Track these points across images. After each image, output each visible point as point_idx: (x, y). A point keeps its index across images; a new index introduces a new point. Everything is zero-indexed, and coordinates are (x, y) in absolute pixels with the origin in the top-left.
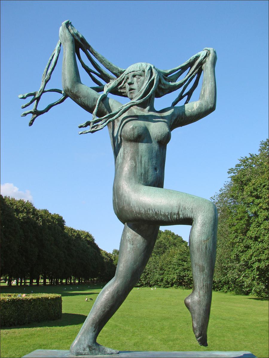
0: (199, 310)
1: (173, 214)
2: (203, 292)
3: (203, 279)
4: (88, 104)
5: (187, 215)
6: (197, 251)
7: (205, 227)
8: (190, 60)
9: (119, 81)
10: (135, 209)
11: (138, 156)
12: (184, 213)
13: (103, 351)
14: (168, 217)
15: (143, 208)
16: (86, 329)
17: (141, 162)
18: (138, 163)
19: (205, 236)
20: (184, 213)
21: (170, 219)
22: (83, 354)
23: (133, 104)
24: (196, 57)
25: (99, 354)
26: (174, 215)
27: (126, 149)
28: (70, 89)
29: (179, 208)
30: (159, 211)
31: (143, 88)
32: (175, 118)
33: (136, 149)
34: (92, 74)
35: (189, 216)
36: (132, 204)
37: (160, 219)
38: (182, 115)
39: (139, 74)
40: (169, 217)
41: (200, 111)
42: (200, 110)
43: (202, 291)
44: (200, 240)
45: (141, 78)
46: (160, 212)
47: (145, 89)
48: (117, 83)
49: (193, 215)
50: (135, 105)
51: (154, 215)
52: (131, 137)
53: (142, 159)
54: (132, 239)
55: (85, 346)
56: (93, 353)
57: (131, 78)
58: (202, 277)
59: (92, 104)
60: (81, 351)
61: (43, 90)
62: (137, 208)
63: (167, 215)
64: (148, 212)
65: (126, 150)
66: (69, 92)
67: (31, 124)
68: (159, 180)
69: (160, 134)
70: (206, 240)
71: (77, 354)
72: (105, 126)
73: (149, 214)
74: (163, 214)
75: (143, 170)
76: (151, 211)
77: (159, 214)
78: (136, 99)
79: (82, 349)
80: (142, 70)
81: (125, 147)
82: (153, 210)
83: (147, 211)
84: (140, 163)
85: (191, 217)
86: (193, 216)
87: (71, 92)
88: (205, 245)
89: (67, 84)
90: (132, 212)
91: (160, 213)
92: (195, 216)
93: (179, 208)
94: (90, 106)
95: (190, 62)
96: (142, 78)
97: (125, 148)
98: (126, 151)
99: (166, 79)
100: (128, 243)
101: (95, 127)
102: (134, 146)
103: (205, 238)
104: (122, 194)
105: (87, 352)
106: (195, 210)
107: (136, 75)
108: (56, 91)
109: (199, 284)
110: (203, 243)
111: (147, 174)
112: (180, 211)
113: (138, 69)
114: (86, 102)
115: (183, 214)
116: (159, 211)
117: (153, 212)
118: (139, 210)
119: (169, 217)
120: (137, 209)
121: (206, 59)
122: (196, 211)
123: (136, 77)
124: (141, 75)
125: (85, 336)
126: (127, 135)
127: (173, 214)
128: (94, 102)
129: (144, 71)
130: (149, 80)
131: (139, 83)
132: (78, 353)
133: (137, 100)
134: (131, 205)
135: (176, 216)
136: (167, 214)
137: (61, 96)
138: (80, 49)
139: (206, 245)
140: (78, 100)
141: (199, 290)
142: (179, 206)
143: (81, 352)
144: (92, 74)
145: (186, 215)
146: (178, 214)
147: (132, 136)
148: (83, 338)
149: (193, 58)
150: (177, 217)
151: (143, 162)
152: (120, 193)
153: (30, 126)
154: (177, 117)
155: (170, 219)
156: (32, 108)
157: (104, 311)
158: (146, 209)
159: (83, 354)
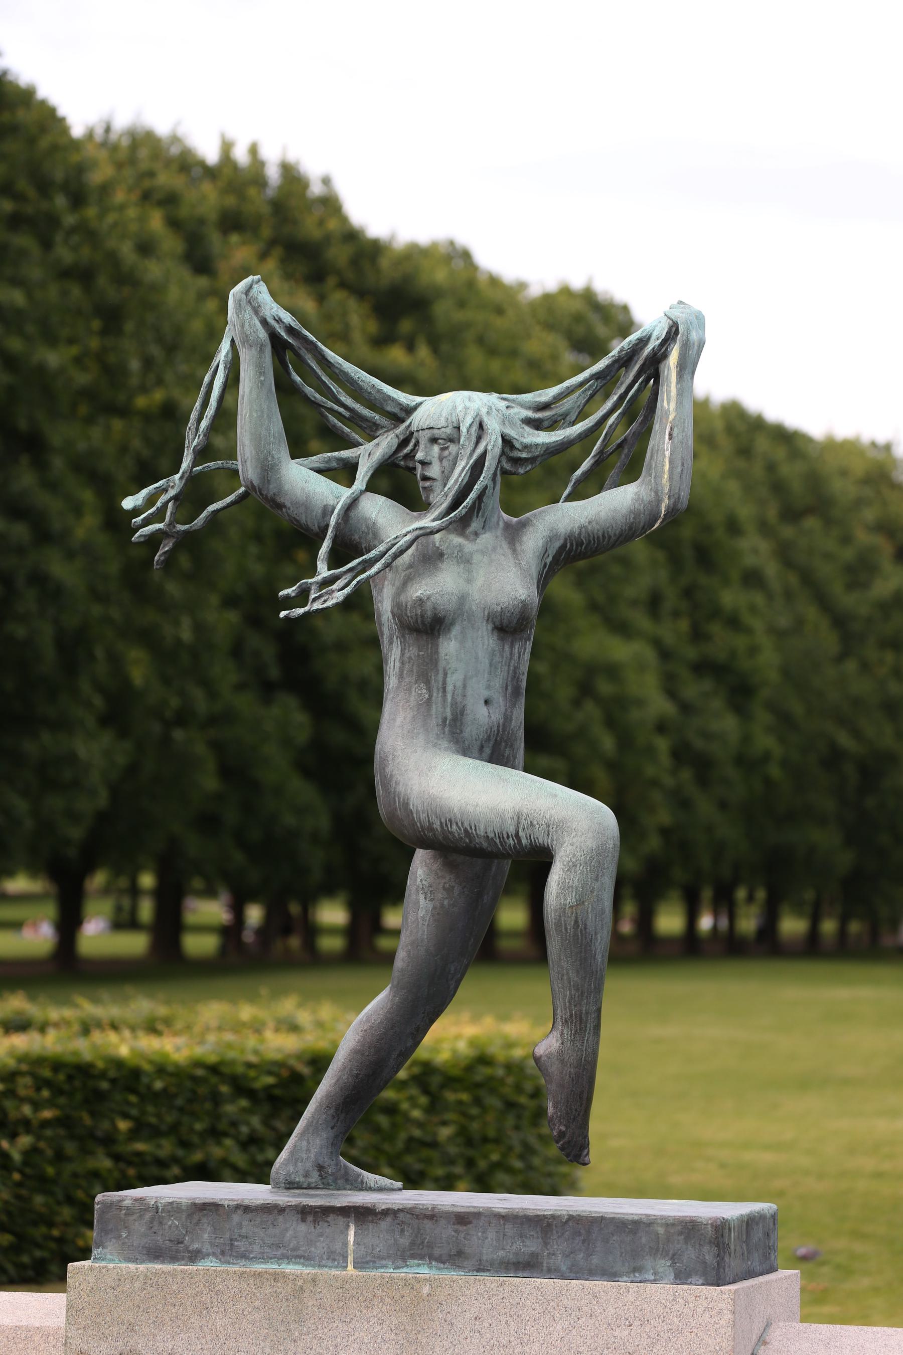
0: (561, 1073)
1: (505, 836)
2: (571, 1030)
3: (571, 998)
4: (309, 523)
5: (537, 841)
6: (556, 930)
7: (576, 872)
8: (621, 350)
9: (402, 438)
10: (420, 818)
11: (438, 671)
12: (530, 836)
13: (356, 1181)
14: (496, 843)
15: (437, 817)
16: (312, 1122)
18: (435, 690)
19: (574, 894)
20: (530, 836)
21: (500, 846)
22: (305, 1185)
23: (421, 532)
24: (638, 339)
25: (345, 1189)
26: (508, 837)
27: (407, 651)
28: (259, 488)
29: (518, 823)
30: (473, 828)
32: (558, 544)
33: (431, 652)
35: (541, 841)
36: (413, 805)
37: (477, 846)
38: (580, 534)
39: (445, 438)
40: (498, 841)
41: (632, 520)
43: (568, 1027)
44: (561, 903)
46: (475, 830)
47: (457, 487)
48: (395, 443)
49: (549, 841)
51: (463, 836)
52: (417, 621)
53: (448, 679)
54: (431, 886)
55: (309, 1165)
56: (328, 1184)
57: (426, 447)
58: (568, 993)
59: (319, 523)
60: (299, 1179)
61: (188, 473)
62: (424, 815)
63: (492, 838)
64: (448, 828)
65: (407, 655)
66: (256, 493)
69: (499, 609)
70: (577, 905)
71: (288, 1186)
73: (451, 833)
74: (482, 834)
75: (448, 710)
76: (454, 827)
77: (472, 833)
79: (301, 1172)
80: (431, 466)
81: (405, 645)
82: (460, 824)
83: (446, 825)
84: (441, 690)
85: (546, 844)
86: (549, 844)
87: (261, 494)
88: (573, 918)
89: (249, 473)
90: (414, 824)
91: (474, 832)
92: (555, 842)
93: (518, 823)
94: (315, 528)
95: (619, 356)
96: (453, 448)
97: (405, 649)
98: (408, 656)
100: (422, 897)
101: (323, 599)
102: (428, 645)
103: (574, 900)
104: (391, 775)
106: (554, 829)
107: (438, 439)
109: (562, 1011)
110: (568, 912)
111: (461, 720)
112: (520, 830)
113: (442, 423)
114: (304, 518)
115: (529, 838)
116: (473, 828)
117: (460, 829)
118: (429, 821)
119: (498, 841)
121: (667, 349)
122: (556, 831)
123: (439, 444)
124: (451, 440)
125: (308, 1140)
126: (408, 617)
127: (505, 836)
128: (323, 518)
129: (458, 428)
131: (445, 463)
132: (290, 1183)
134: (411, 807)
135: (513, 840)
136: (491, 835)
139: (576, 917)
140: (283, 513)
143: (297, 1180)
145: (535, 840)
146: (517, 835)
147: (419, 621)
148: (305, 1143)
149: (629, 344)
150: (515, 843)
151: (450, 688)
152: (387, 770)
154: (566, 540)
155: (500, 846)
157: (357, 1075)
158: (443, 821)
159: (304, 1186)
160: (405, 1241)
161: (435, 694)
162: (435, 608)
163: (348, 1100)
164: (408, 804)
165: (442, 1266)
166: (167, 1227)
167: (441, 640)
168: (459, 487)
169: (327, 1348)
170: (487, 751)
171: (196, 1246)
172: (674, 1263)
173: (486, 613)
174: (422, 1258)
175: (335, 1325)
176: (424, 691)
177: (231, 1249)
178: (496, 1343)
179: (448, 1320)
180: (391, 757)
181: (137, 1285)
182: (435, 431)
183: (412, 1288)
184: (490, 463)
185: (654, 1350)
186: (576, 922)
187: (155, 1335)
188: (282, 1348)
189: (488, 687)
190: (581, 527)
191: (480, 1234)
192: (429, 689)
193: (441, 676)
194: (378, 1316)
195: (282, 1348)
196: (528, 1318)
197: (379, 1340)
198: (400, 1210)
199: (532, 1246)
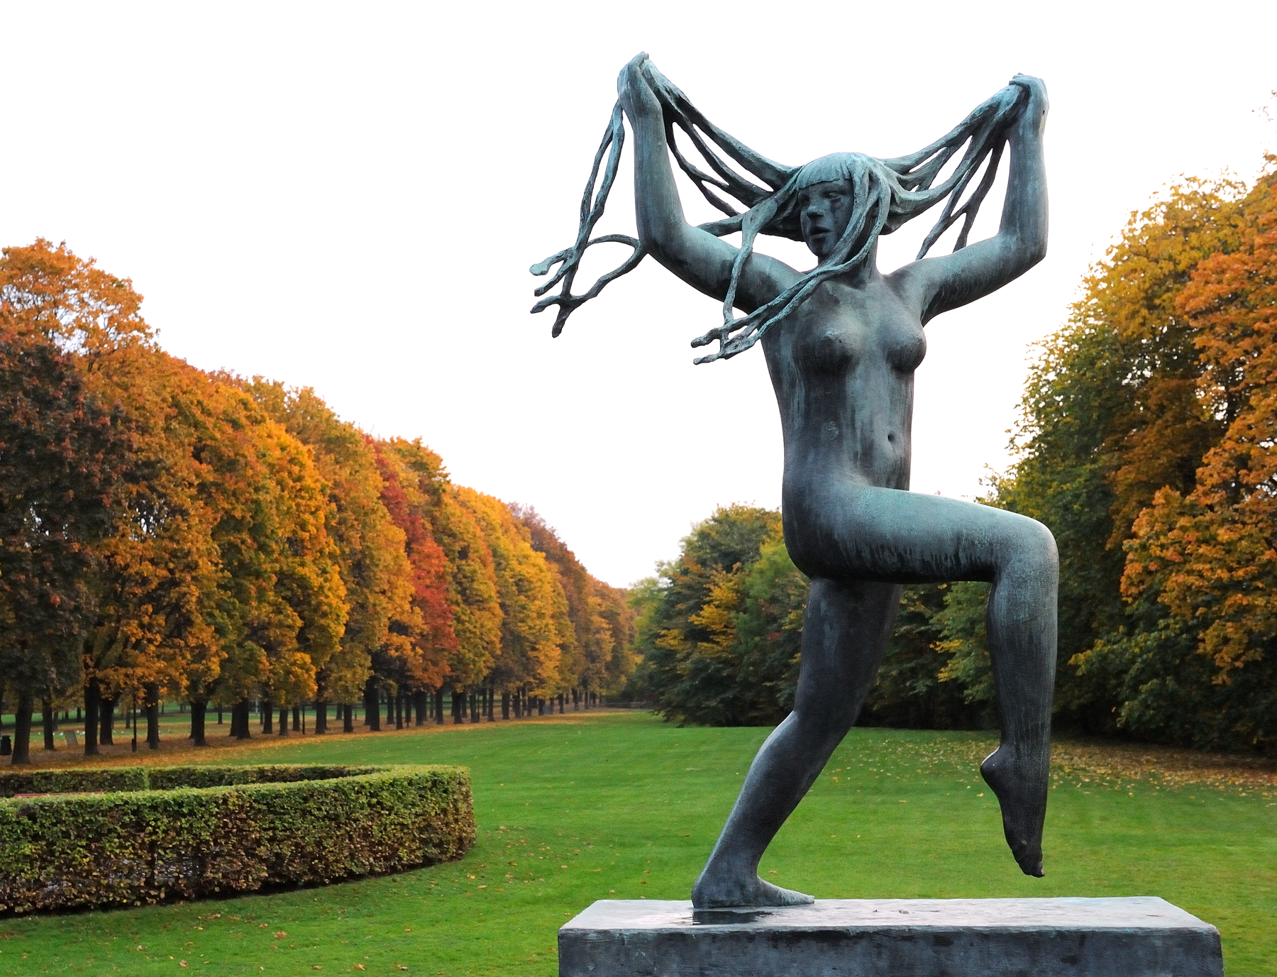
22: (728, 904)
31: (849, 228)
67: (557, 331)
137: (628, 252)
151: (858, 424)
156: (557, 291)
170: (893, 483)
182: (827, 185)
190: (955, 275)
193: (849, 415)
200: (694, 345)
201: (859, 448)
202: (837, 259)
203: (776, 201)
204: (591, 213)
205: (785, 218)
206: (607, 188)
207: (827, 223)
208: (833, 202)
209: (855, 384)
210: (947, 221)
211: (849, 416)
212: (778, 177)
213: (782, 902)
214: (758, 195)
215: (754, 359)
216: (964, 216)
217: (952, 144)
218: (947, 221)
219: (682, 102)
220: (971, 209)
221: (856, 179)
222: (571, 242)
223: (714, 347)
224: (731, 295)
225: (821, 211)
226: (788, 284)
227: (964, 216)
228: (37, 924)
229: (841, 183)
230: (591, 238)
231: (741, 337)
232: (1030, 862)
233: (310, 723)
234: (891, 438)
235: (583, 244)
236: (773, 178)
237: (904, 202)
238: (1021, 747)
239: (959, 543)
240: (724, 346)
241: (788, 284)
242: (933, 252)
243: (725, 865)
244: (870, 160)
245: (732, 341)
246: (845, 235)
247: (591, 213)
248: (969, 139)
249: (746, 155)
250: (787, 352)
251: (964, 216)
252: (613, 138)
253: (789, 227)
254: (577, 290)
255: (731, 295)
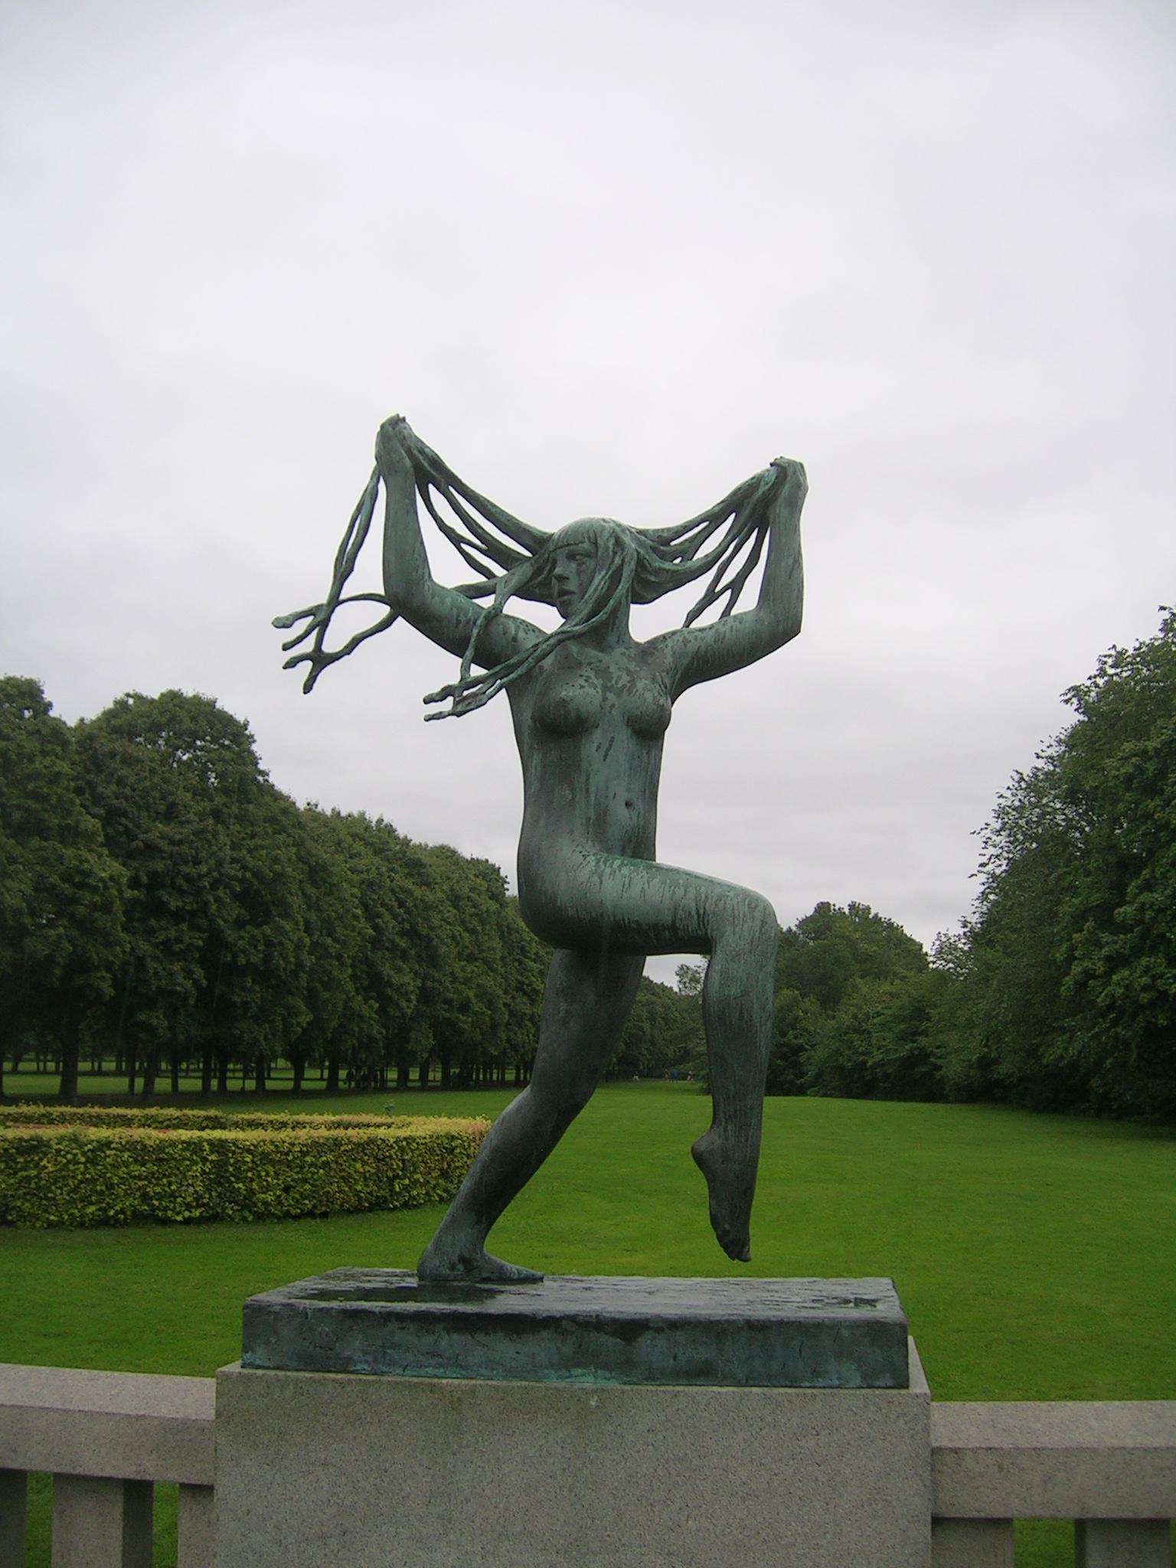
17: (587, 791)
22: (452, 1278)
31: (591, 590)
34: (464, 546)
38: (706, 652)
42: (754, 635)
45: (588, 564)
47: (596, 594)
50: (568, 639)
53: (591, 781)
67: (308, 688)
68: (639, 833)
72: (499, 689)
78: (574, 623)
92: (715, 933)
96: (590, 563)
99: (663, 556)
101: (467, 702)
105: (459, 1273)
108: (373, 597)
120: (571, 912)
124: (588, 555)
130: (609, 568)
133: (575, 626)
137: (384, 610)
138: (431, 487)
141: (726, 1122)
142: (676, 909)
144: (464, 546)
151: (592, 789)
153: (305, 693)
154: (693, 658)
156: (308, 646)
160: (568, 1349)
161: (578, 795)
162: (578, 709)
163: (131, 701)
164: (556, 901)
165: (608, 1375)
166: (316, 1333)
167: (583, 742)
168: (599, 595)
169: (489, 1461)
170: (629, 851)
171: (347, 1353)
172: (860, 1366)
173: (626, 718)
174: (585, 1366)
175: (496, 1438)
176: (567, 792)
177: (384, 1357)
178: (671, 1456)
179: (619, 1433)
180: (536, 856)
181: (288, 1393)
182: (571, 548)
183: (579, 1400)
184: (627, 573)
185: (844, 1459)
186: (741, 1013)
187: (307, 1445)
188: (439, 1460)
189: (628, 790)
191: (649, 1341)
192: (573, 790)
193: (583, 779)
194: (543, 1429)
195: (439, 1460)
196: (705, 1430)
197: (545, 1453)
198: (562, 1318)
199: (703, 1353)
200: (426, 701)
201: (592, 813)
202: (577, 619)
203: (532, 565)
204: (344, 567)
205: (540, 582)
206: (359, 545)
207: (572, 585)
208: (580, 565)
209: (591, 747)
210: (710, 597)
211: (584, 781)
212: (536, 541)
213: (505, 1278)
214: (517, 560)
215: (500, 705)
216: (728, 593)
217: (714, 519)
218: (710, 597)
219: (436, 463)
220: (736, 586)
221: (601, 542)
222: (323, 599)
223: (448, 704)
224: (469, 653)
225: (566, 574)
226: (529, 641)
227: (729, 592)
228: (951, 1441)
229: (586, 545)
230: (342, 597)
231: (474, 695)
232: (735, 1245)
233: (9, 1060)
234: (628, 804)
235: (335, 601)
236: (529, 542)
237: (658, 572)
238: (729, 1127)
239: (676, 913)
240: (456, 704)
241: (529, 641)
242: (697, 624)
243: (450, 1238)
244: (619, 525)
245: (466, 698)
246: (586, 597)
247: (344, 567)
248: (733, 516)
249: (503, 519)
250: (527, 715)
251: (728, 593)
252: (371, 495)
253: (544, 592)
254: (330, 646)
255: (469, 653)
